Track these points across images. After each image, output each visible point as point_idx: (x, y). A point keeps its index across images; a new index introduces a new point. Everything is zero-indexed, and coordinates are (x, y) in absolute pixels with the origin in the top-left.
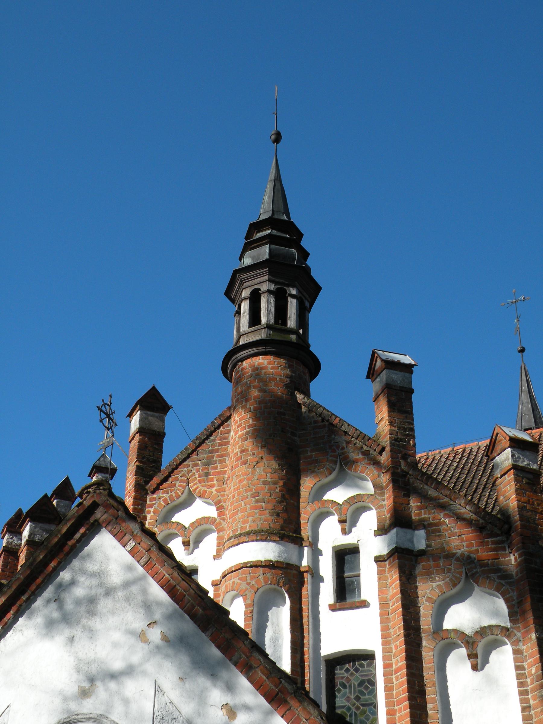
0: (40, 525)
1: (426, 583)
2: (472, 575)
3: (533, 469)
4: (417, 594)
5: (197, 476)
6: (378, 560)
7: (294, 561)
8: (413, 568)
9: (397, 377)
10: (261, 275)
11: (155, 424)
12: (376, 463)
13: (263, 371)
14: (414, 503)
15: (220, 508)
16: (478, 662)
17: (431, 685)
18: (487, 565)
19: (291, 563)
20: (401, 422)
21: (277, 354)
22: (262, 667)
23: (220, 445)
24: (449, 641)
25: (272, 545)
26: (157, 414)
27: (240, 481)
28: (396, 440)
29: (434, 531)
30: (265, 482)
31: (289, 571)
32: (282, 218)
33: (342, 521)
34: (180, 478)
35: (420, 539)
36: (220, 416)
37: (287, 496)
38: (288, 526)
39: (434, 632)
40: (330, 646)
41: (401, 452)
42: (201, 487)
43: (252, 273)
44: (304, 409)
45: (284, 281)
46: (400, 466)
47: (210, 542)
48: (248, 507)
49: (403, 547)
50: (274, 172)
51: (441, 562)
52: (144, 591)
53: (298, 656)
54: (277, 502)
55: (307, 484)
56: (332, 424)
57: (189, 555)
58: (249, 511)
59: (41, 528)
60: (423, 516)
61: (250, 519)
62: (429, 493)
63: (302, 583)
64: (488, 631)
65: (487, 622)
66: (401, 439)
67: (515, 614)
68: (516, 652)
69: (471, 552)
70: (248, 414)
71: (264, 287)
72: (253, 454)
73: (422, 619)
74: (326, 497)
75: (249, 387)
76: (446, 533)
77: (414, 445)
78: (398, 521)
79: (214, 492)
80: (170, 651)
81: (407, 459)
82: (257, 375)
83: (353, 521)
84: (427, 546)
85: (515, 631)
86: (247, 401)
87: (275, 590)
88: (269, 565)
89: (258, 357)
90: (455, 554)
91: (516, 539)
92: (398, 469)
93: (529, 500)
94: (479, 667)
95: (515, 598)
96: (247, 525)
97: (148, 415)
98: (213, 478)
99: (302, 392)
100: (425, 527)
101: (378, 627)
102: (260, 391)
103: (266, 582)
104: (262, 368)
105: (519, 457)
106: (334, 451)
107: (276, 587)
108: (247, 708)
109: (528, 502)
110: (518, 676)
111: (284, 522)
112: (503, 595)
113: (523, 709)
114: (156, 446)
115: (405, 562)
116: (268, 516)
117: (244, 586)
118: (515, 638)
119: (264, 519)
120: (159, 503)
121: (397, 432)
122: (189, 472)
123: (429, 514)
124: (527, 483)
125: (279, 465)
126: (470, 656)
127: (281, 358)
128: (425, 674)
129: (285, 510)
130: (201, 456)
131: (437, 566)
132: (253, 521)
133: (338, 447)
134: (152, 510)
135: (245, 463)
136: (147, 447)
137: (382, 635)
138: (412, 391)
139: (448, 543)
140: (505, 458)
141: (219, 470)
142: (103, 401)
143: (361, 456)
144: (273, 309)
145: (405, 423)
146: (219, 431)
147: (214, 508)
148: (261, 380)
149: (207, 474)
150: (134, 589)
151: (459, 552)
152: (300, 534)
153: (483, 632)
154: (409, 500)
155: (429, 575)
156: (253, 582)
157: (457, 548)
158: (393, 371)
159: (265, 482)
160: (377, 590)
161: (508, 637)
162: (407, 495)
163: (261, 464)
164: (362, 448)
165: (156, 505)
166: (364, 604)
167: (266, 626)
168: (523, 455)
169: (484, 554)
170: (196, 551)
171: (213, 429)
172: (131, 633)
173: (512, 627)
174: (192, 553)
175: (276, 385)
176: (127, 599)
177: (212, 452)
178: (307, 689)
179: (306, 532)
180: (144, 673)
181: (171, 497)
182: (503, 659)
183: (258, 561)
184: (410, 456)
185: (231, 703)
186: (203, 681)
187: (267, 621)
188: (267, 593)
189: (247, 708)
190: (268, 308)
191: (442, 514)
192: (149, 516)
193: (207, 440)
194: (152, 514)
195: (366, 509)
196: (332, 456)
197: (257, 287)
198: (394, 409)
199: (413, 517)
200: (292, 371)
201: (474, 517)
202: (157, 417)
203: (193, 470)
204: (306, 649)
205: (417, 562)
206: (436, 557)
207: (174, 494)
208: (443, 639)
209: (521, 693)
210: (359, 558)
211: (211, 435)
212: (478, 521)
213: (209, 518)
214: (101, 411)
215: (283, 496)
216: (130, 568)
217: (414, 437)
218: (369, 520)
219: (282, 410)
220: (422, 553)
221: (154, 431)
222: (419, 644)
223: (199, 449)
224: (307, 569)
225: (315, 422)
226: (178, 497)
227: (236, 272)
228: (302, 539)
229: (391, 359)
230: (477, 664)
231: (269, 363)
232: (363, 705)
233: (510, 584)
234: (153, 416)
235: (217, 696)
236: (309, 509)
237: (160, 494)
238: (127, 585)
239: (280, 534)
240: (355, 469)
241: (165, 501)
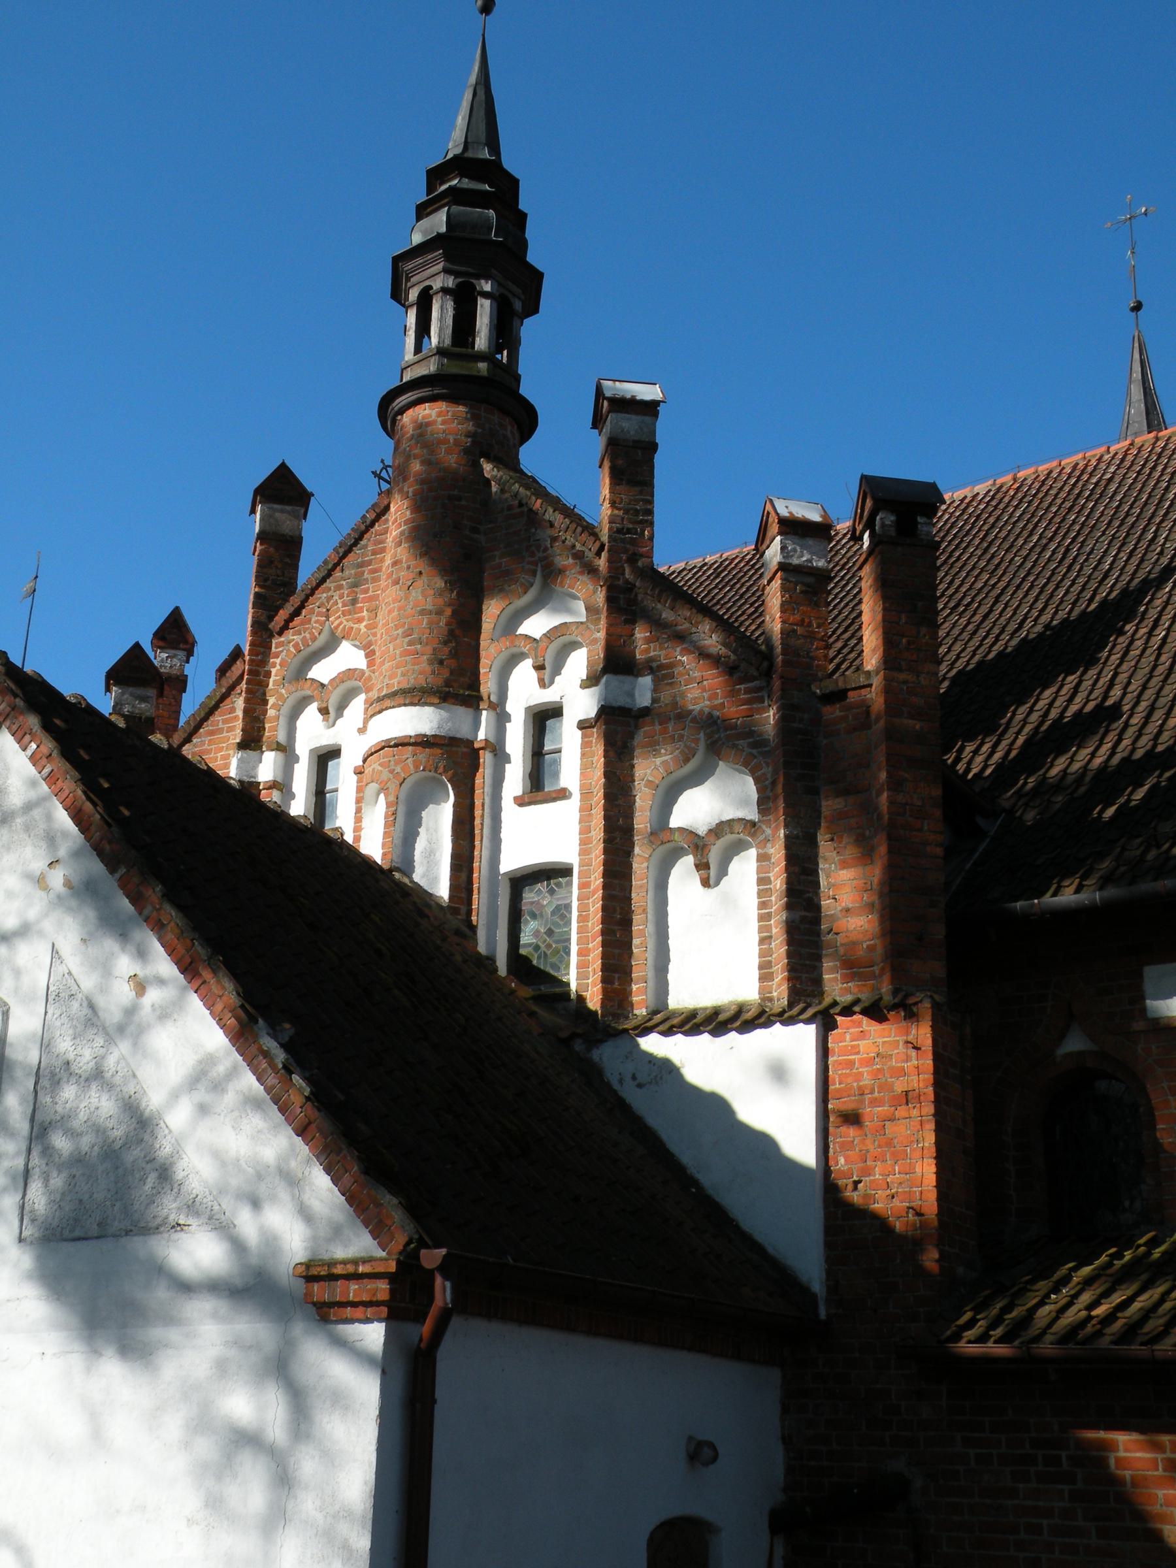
0: (131, 689)
1: (647, 758)
2: (716, 742)
3: (817, 569)
4: (632, 776)
5: (340, 605)
6: (583, 725)
7: (464, 732)
8: (631, 736)
9: (629, 424)
10: (434, 261)
11: (285, 523)
12: (591, 570)
13: (429, 429)
14: (641, 634)
15: (369, 655)
16: (710, 875)
17: (640, 911)
18: (735, 727)
19: (458, 736)
21: (452, 398)
22: (172, 924)
23: (374, 553)
24: (677, 844)
25: (428, 710)
26: (288, 508)
27: (390, 612)
28: (619, 531)
29: (665, 677)
30: (423, 612)
31: (454, 749)
32: (482, 157)
33: (539, 668)
34: (317, 610)
35: (643, 691)
36: (374, 506)
37: (457, 632)
38: (457, 677)
39: (652, 833)
40: (515, 856)
41: (626, 551)
43: (420, 260)
44: (494, 488)
46: (623, 574)
47: (357, 707)
48: (398, 652)
49: (615, 704)
50: (476, 68)
51: (671, 726)
52: (49, 817)
53: (464, 876)
54: (440, 643)
55: (492, 611)
56: (531, 510)
57: (329, 727)
58: (398, 659)
59: (131, 695)
60: (652, 654)
61: (399, 671)
62: (664, 616)
63: (475, 766)
64: (727, 829)
65: (730, 814)
67: (764, 804)
68: (762, 858)
69: (714, 707)
70: (405, 502)
71: (437, 284)
72: (408, 567)
73: (637, 814)
74: (522, 630)
75: (408, 458)
76: (682, 679)
77: (651, 538)
78: (615, 663)
79: (363, 630)
80: (74, 903)
81: (637, 561)
82: (421, 435)
83: (550, 670)
84: (654, 701)
85: (764, 827)
86: (405, 479)
87: (434, 778)
88: (423, 742)
90: (691, 711)
91: (777, 684)
92: (619, 579)
93: (803, 621)
94: (712, 882)
95: (769, 776)
96: (395, 681)
98: (362, 608)
99: (497, 461)
100: (652, 671)
101: (576, 828)
102: (422, 463)
103: (416, 767)
104: (428, 424)
105: (795, 550)
106: (533, 554)
107: (432, 774)
108: (161, 981)
109: (801, 623)
110: (760, 894)
111: (452, 673)
112: (752, 773)
113: (762, 941)
114: (288, 560)
115: (618, 728)
116: (425, 666)
117: (385, 775)
118: (762, 837)
119: (419, 671)
120: (288, 650)
122: (329, 598)
123: (661, 649)
124: (802, 592)
126: (698, 867)
127: (459, 404)
128: (633, 895)
129: (454, 654)
130: (347, 573)
131: (665, 731)
132: (403, 675)
133: (538, 547)
134: (278, 661)
135: (396, 582)
136: (272, 562)
137: (581, 839)
138: (653, 447)
139: (683, 695)
140: (774, 553)
141: (370, 593)
142: (382, 461)
143: (571, 561)
144: (449, 321)
145: (637, 501)
146: (373, 530)
147: (361, 654)
148: (426, 445)
149: (354, 601)
150: (37, 813)
151: (697, 707)
152: (479, 691)
153: (719, 829)
154: (634, 629)
155: (653, 747)
156: (398, 769)
157: (695, 701)
159: (423, 612)
160: (579, 772)
161: (753, 835)
162: (632, 621)
163: (419, 583)
164: (574, 546)
165: (284, 653)
166: (563, 794)
167: (418, 834)
168: (802, 547)
169: (733, 711)
170: (339, 722)
171: (363, 527)
172: (28, 876)
173: (760, 821)
174: (333, 725)
175: (449, 451)
176: (27, 829)
177: (362, 565)
178: (475, 923)
179: (488, 686)
180: (41, 934)
181: (304, 640)
182: (744, 869)
183: (406, 737)
184: (642, 556)
185: (141, 974)
186: (110, 944)
187: (420, 825)
188: (418, 784)
189: (161, 981)
190: (441, 319)
191: (678, 649)
192: (274, 671)
194: (278, 667)
195: (573, 646)
196: (529, 563)
197: (427, 283)
198: (622, 480)
199: (638, 657)
200: (477, 425)
201: (723, 651)
202: (289, 513)
203: (334, 595)
204: (476, 865)
205: (637, 727)
206: (664, 720)
207: (308, 636)
208: (662, 843)
209: (761, 918)
210: (561, 727)
211: (361, 537)
212: (729, 657)
213: (355, 670)
214: (380, 478)
215: (451, 633)
216: (33, 784)
217: (651, 524)
218: (578, 664)
219: (456, 492)
220: (645, 712)
221: (283, 535)
222: (629, 853)
224: (482, 745)
225: (510, 508)
226: (314, 639)
227: (397, 261)
228: (480, 698)
229: (620, 394)
230: (708, 878)
231: (439, 414)
232: (557, 942)
233: (765, 754)
234: (282, 511)
235: (125, 965)
236: (492, 650)
237: (289, 635)
238: (28, 807)
239: (440, 692)
240: (561, 582)
241: (296, 646)
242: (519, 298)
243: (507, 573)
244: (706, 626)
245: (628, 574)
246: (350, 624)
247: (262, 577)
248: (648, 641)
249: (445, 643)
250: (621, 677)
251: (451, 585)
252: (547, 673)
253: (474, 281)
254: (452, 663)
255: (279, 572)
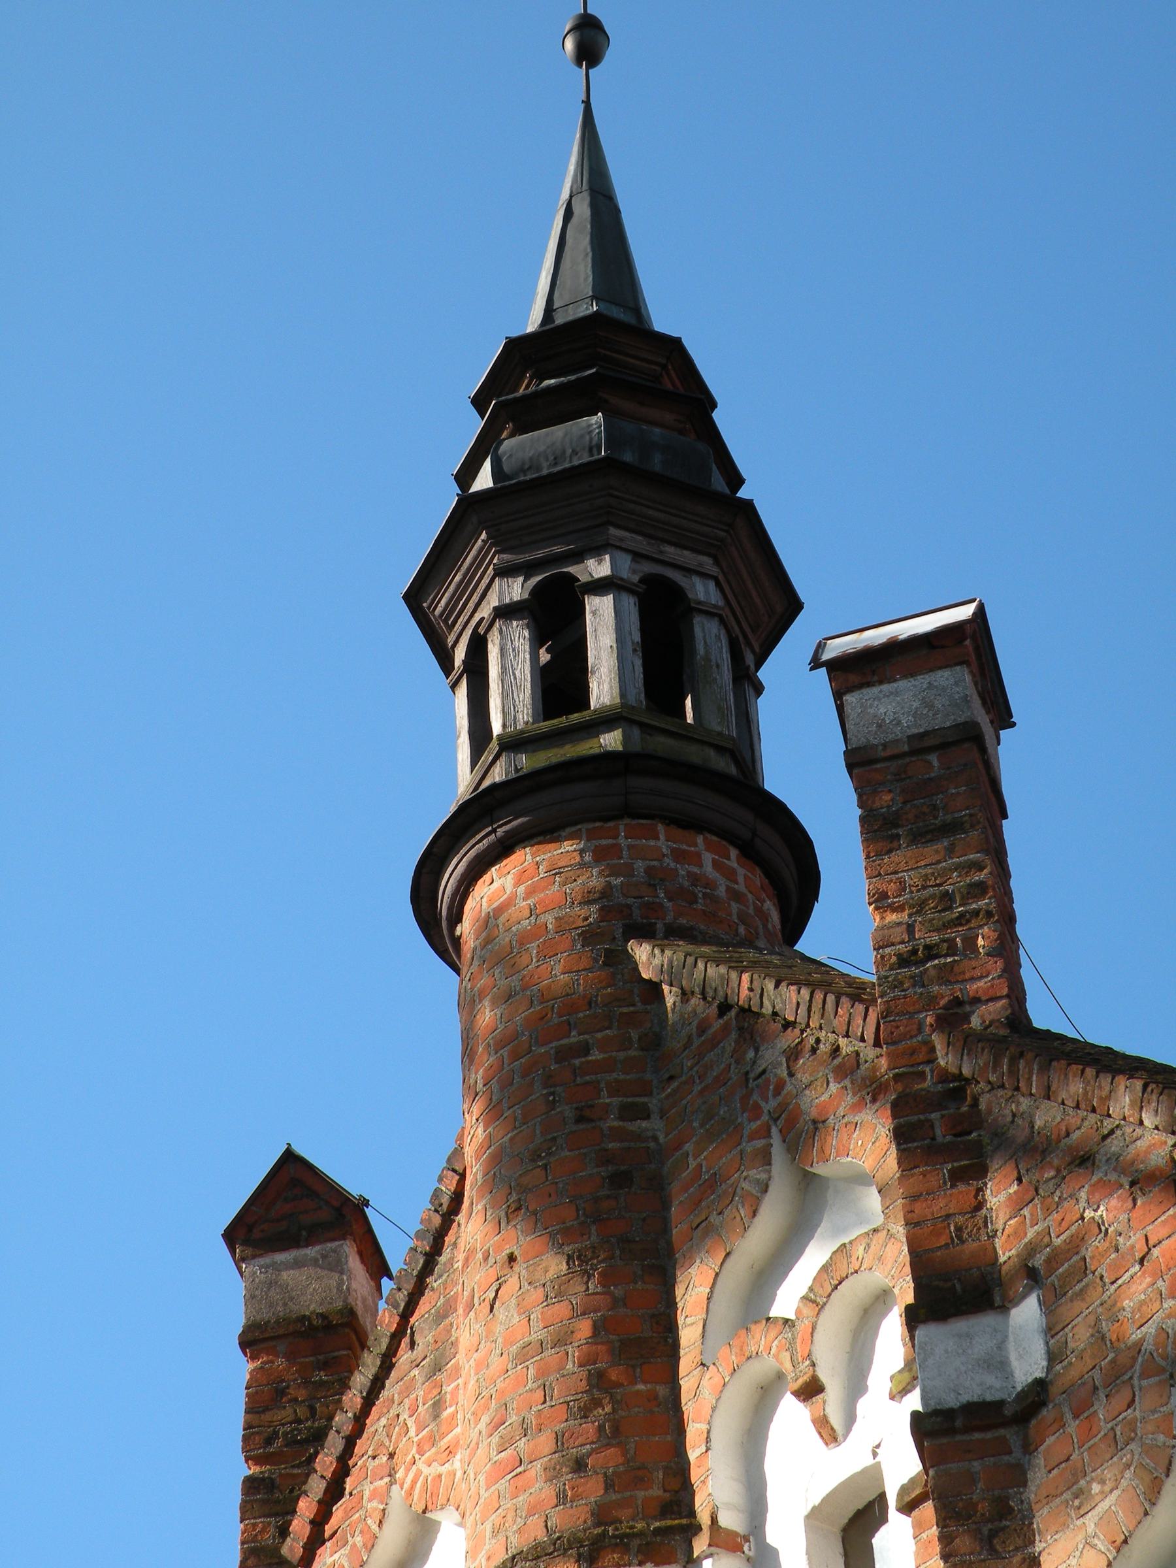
1: (1065, 1526)
8: (1018, 1475)
20: (926, 877)
21: (542, 832)
26: (311, 1252)
37: (614, 1375)
42: (426, 1471)
45: (558, 549)
46: (932, 1060)
49: (952, 1401)
51: (1101, 1411)
60: (1031, 1233)
66: (927, 947)
81: (966, 1018)
84: (1053, 1357)
89: (486, 877)
90: (1138, 1346)
97: (277, 1268)
100: (1033, 1276)
111: (609, 1485)
114: (322, 1376)
116: (541, 1490)
121: (910, 929)
123: (1048, 1211)
125: (570, 1258)
127: (558, 840)
129: (613, 1433)
152: (692, 1513)
158: (875, 690)
164: (836, 1050)
179: (715, 1490)
193: (431, 1273)
205: (1029, 1448)
215: (598, 1382)
219: (574, 1038)
223: (412, 1320)
227: (414, 598)
234: (297, 1264)
242: (704, 575)
243: (713, 1183)
244: (1124, 1098)
245: (945, 1059)
246: (436, 1469)
247: (258, 1440)
248: (1018, 1206)
249: (585, 1413)
250: (960, 1325)
251: (580, 1261)
252: (832, 1400)
253: (572, 569)
254: (611, 1458)
255: (302, 1412)
